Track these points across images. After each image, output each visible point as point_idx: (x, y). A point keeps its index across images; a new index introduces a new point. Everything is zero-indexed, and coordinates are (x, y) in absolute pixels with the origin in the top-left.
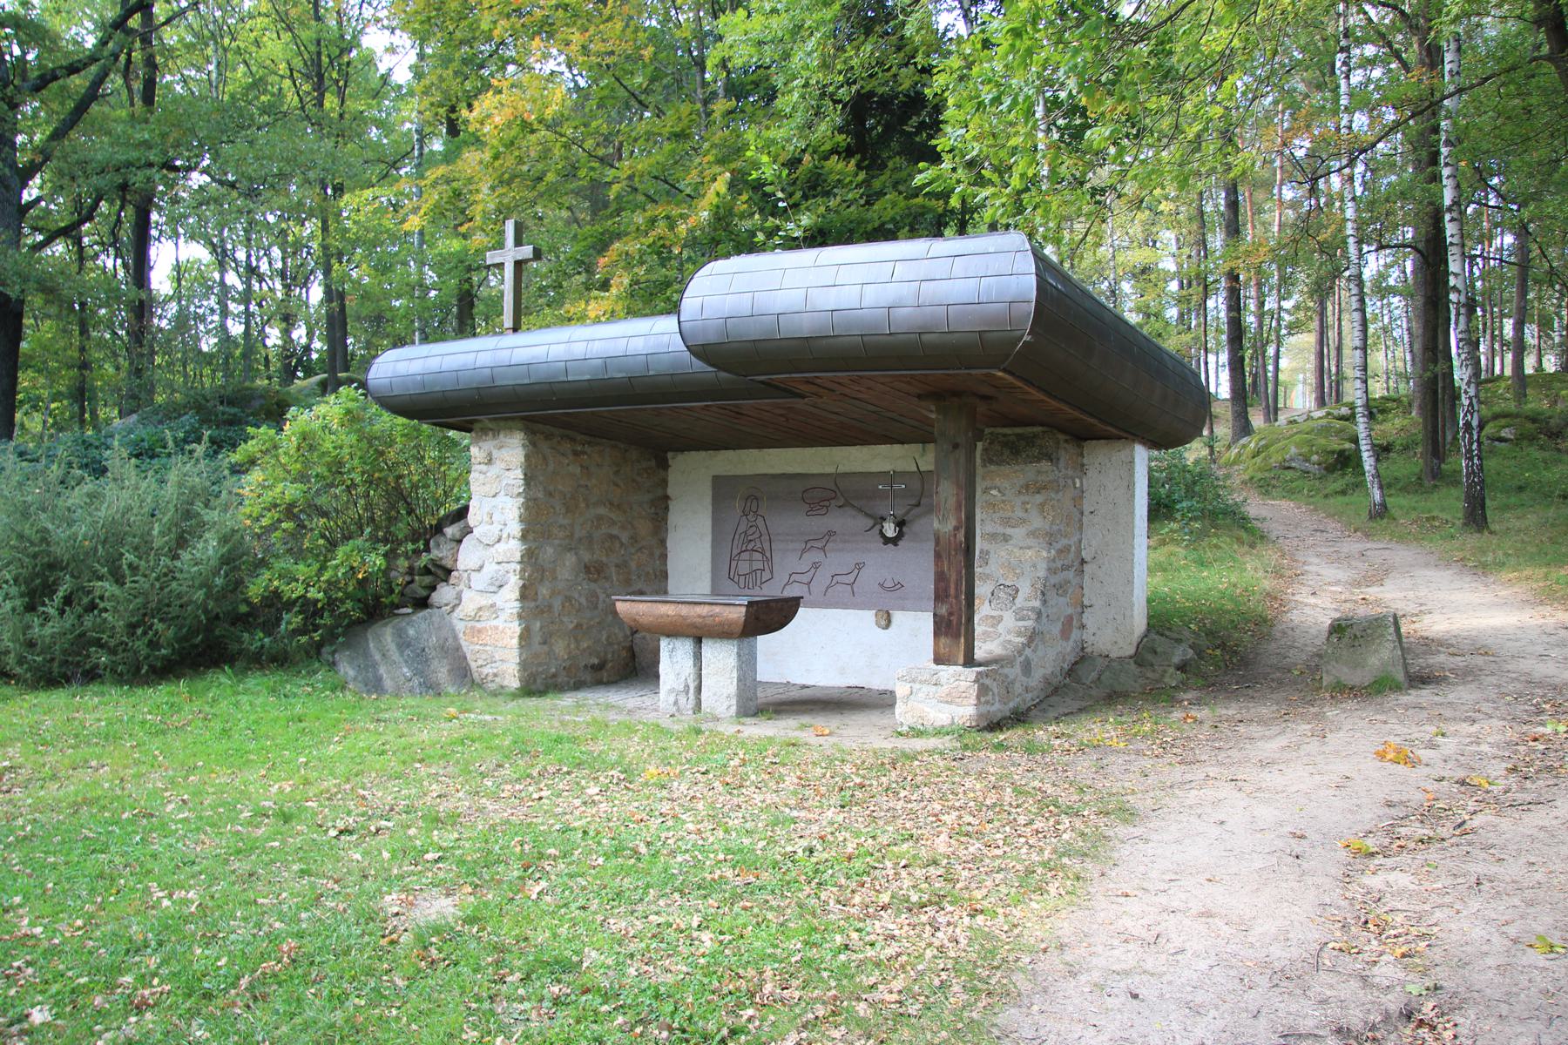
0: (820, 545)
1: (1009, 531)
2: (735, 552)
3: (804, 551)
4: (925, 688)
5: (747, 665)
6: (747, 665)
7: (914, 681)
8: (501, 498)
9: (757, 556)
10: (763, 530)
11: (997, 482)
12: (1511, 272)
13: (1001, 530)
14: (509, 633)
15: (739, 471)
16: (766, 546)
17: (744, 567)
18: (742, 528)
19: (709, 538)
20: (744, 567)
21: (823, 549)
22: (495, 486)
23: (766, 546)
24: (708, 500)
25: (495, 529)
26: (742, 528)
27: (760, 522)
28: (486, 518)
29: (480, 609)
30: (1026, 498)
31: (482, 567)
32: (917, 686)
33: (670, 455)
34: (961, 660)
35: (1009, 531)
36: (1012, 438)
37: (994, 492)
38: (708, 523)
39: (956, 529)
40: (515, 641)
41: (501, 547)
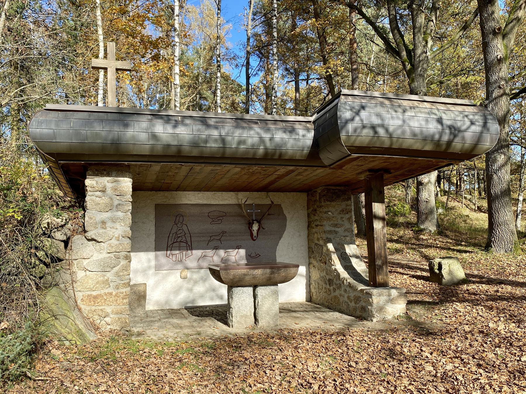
1: (337, 229)
2: (170, 243)
3: (209, 241)
5: (417, 179)
6: (417, 179)
10: (187, 232)
11: (330, 209)
12: (452, 170)
13: (333, 229)
18: (174, 231)
19: (153, 237)
21: (220, 240)
24: (152, 217)
26: (174, 231)
27: (185, 228)
30: (342, 216)
33: (346, 246)
35: (337, 229)
37: (329, 213)
38: (153, 228)
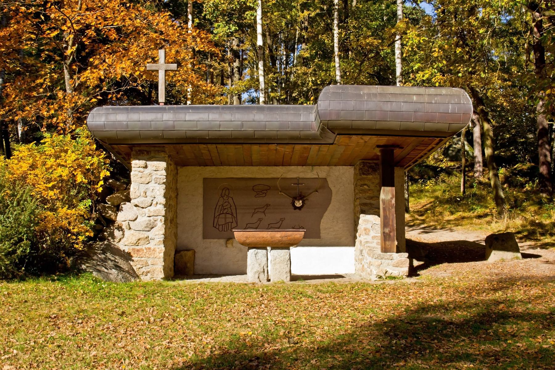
0: (262, 210)
2: (217, 214)
3: (254, 213)
4: (387, 261)
7: (382, 259)
8: (152, 185)
9: (228, 216)
14: (158, 250)
15: (219, 176)
16: (234, 211)
17: (222, 221)
18: (221, 203)
20: (222, 221)
21: (264, 212)
22: (149, 179)
23: (234, 211)
25: (149, 200)
28: (142, 194)
29: (139, 240)
31: (136, 219)
32: (383, 261)
34: (395, 250)
36: (373, 164)
39: (392, 198)
40: (162, 255)
41: (152, 208)
